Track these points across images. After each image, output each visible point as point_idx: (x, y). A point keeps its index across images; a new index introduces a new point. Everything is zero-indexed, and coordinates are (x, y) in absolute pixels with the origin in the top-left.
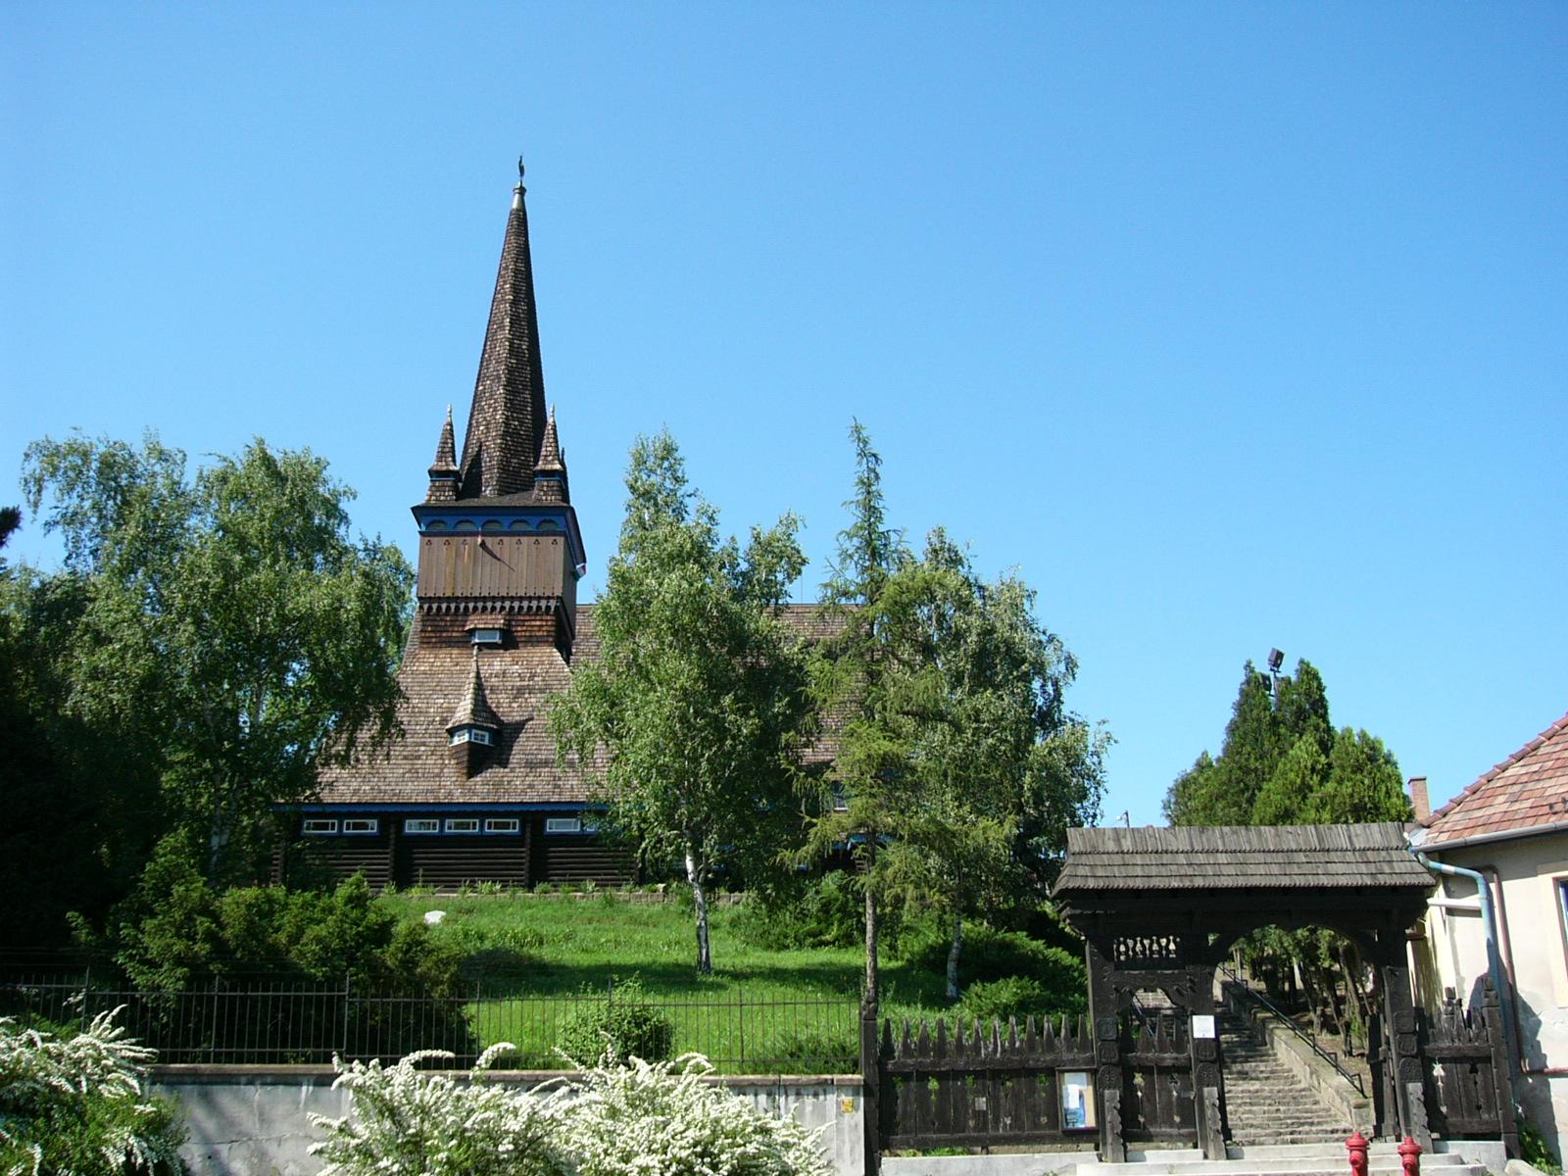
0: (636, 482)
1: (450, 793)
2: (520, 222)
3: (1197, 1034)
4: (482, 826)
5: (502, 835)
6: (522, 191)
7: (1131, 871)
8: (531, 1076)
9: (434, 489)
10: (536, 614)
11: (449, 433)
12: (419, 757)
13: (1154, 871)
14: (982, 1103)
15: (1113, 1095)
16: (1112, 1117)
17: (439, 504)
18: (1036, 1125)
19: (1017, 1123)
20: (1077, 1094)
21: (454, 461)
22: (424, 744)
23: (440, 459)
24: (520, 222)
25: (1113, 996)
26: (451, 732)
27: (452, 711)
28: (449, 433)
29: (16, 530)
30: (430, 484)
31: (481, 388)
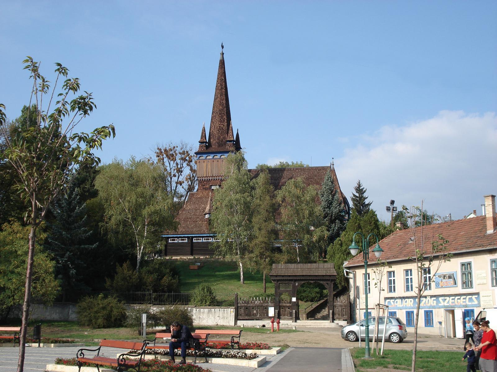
0: (236, 153)
1: (204, 231)
2: (222, 63)
3: (293, 298)
4: (178, 240)
5: (173, 243)
6: (223, 54)
7: (282, 272)
8: (231, 274)
9: (200, 147)
10: (208, 181)
11: (204, 130)
12: (197, 222)
13: (286, 272)
14: (255, 312)
15: (277, 311)
16: (277, 314)
17: (201, 152)
18: (264, 316)
19: (261, 315)
20: (271, 312)
21: (206, 138)
22: (198, 218)
23: (201, 138)
24: (222, 63)
25: (278, 294)
26: (205, 214)
27: (205, 208)
28: (204, 130)
29: (137, 159)
30: (199, 145)
31: (306, 270)
